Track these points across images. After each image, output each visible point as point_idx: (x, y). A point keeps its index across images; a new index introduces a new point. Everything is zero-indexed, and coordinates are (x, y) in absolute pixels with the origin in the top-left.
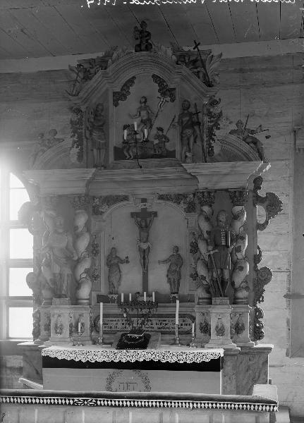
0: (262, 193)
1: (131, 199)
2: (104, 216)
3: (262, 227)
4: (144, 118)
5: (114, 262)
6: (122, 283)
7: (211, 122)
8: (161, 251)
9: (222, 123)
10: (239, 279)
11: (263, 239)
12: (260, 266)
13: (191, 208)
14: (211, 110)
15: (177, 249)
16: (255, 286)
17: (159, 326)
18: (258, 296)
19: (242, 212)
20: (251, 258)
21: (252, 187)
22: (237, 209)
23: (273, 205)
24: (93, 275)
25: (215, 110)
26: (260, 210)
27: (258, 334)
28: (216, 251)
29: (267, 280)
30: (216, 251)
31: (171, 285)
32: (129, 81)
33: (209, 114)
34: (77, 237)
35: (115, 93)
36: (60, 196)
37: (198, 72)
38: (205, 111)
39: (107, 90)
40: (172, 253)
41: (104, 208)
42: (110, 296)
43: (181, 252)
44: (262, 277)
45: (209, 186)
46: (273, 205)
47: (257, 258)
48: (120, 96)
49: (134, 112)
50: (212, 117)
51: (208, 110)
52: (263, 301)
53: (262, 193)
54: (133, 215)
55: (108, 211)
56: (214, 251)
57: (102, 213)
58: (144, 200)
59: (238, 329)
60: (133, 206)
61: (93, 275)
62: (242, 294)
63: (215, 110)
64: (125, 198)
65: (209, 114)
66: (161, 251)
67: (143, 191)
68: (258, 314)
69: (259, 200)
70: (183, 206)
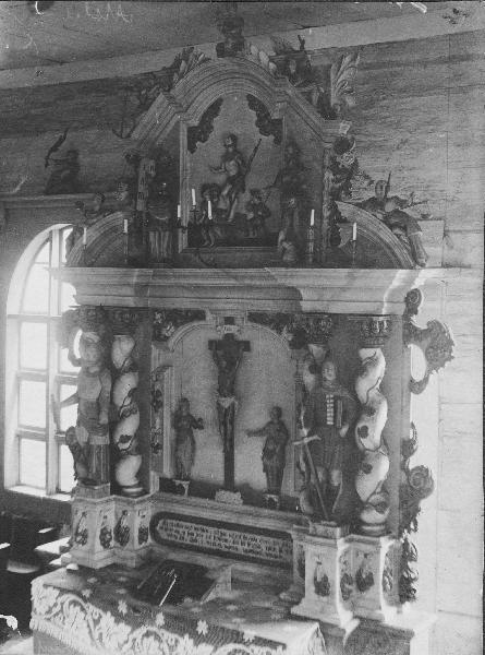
0: (419, 321)
1: (209, 316)
2: (171, 343)
3: (416, 387)
4: (232, 174)
5: (186, 424)
6: (197, 462)
7: (338, 181)
8: (255, 415)
9: (357, 182)
10: (367, 486)
11: (421, 409)
12: (413, 463)
13: (299, 342)
14: (338, 159)
15: (278, 412)
16: (403, 502)
17: (246, 547)
18: (409, 517)
19: (373, 361)
20: (396, 445)
21: (401, 309)
22: (365, 353)
23: (438, 346)
24: (145, 445)
25: (346, 160)
26: (416, 355)
27: (404, 591)
28: (315, 437)
29: (425, 492)
30: (315, 437)
31: (267, 475)
32: (212, 106)
33: (335, 168)
34: (115, 375)
35: (191, 130)
36: (101, 308)
37: (310, 92)
38: (327, 162)
39: (176, 128)
40: (269, 419)
41: (168, 330)
42: (178, 482)
43: (288, 419)
44: (410, 494)
45: (319, 307)
46: (438, 346)
47: (408, 447)
48: (198, 134)
49: (217, 161)
50: (340, 172)
51: (333, 159)
52: (416, 530)
53: (419, 321)
54: (211, 343)
55: (175, 335)
56: (311, 438)
57: (166, 339)
58: (230, 321)
59: (363, 582)
60: (208, 331)
61: (145, 445)
62: (371, 516)
63: (346, 160)
64: (199, 315)
65: (335, 168)
66: (255, 415)
67: (231, 304)
68: (405, 555)
69: (412, 334)
70: (287, 336)
